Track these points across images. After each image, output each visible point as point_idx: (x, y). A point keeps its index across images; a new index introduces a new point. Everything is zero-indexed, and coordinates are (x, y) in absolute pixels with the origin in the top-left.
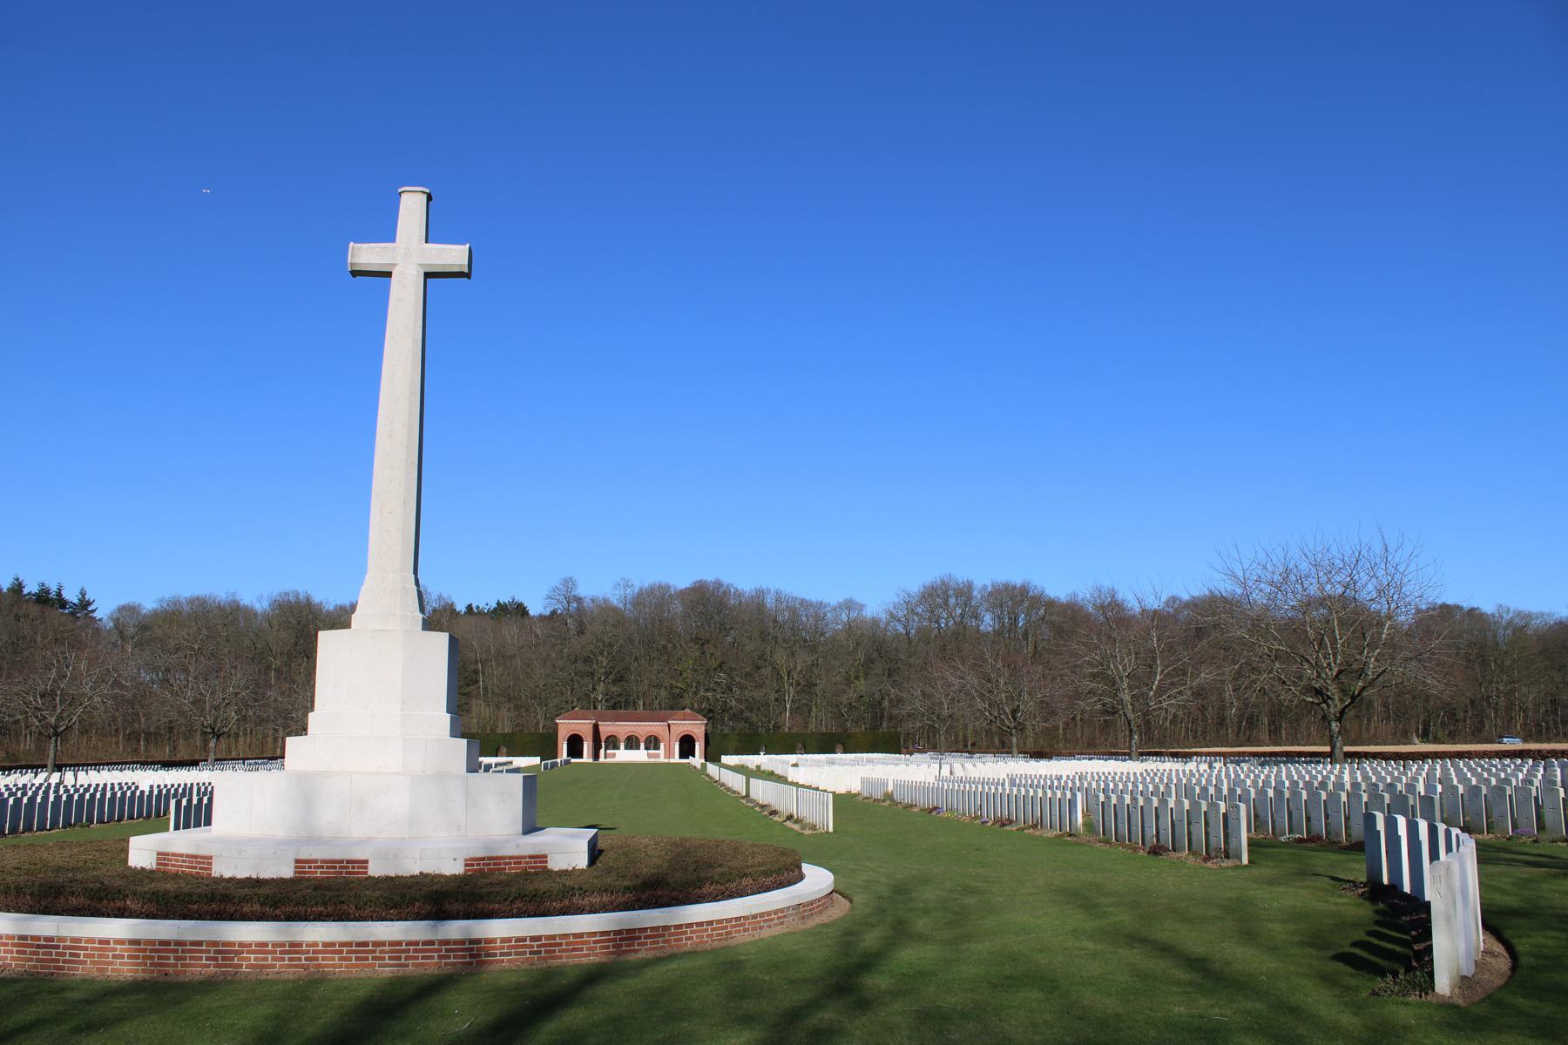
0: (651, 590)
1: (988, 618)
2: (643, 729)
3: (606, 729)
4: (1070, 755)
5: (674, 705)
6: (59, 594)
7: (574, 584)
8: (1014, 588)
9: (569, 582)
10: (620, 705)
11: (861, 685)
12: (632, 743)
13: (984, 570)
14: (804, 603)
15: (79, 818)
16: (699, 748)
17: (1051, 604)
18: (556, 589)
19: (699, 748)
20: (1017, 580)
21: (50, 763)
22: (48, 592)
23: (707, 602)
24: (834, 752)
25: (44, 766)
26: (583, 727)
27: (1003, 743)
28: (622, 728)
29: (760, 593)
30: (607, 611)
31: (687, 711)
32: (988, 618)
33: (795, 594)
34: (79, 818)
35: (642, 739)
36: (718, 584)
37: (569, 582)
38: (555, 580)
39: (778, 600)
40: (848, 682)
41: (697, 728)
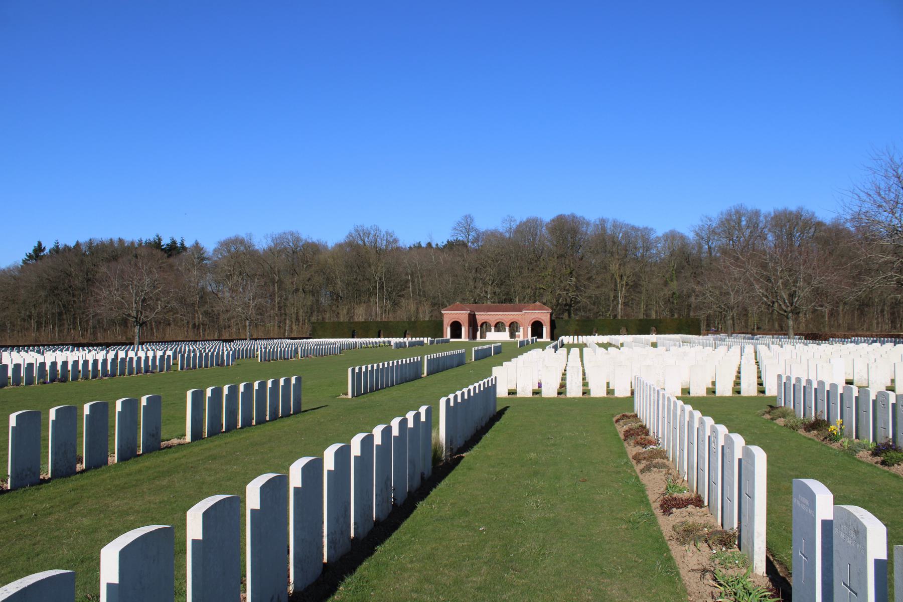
0: (528, 221)
1: (770, 237)
2: (507, 317)
3: (481, 317)
4: (669, 333)
5: (534, 298)
6: (182, 244)
7: (472, 220)
8: (791, 213)
9: (468, 219)
10: (506, 301)
11: (674, 285)
12: (499, 327)
13: (768, 199)
14: (634, 228)
15: (188, 365)
16: (546, 331)
17: (820, 224)
18: (459, 223)
19: (546, 331)
20: (793, 207)
21: (137, 340)
22: (174, 242)
23: (566, 230)
24: (648, 333)
25: (132, 344)
26: (462, 316)
27: (781, 328)
28: (492, 317)
29: (603, 221)
30: (493, 235)
31: (538, 303)
32: (770, 237)
33: (627, 222)
34: (188, 365)
35: (493, 324)
36: (574, 216)
37: (468, 219)
38: (458, 217)
39: (615, 226)
40: (666, 284)
41: (544, 316)
